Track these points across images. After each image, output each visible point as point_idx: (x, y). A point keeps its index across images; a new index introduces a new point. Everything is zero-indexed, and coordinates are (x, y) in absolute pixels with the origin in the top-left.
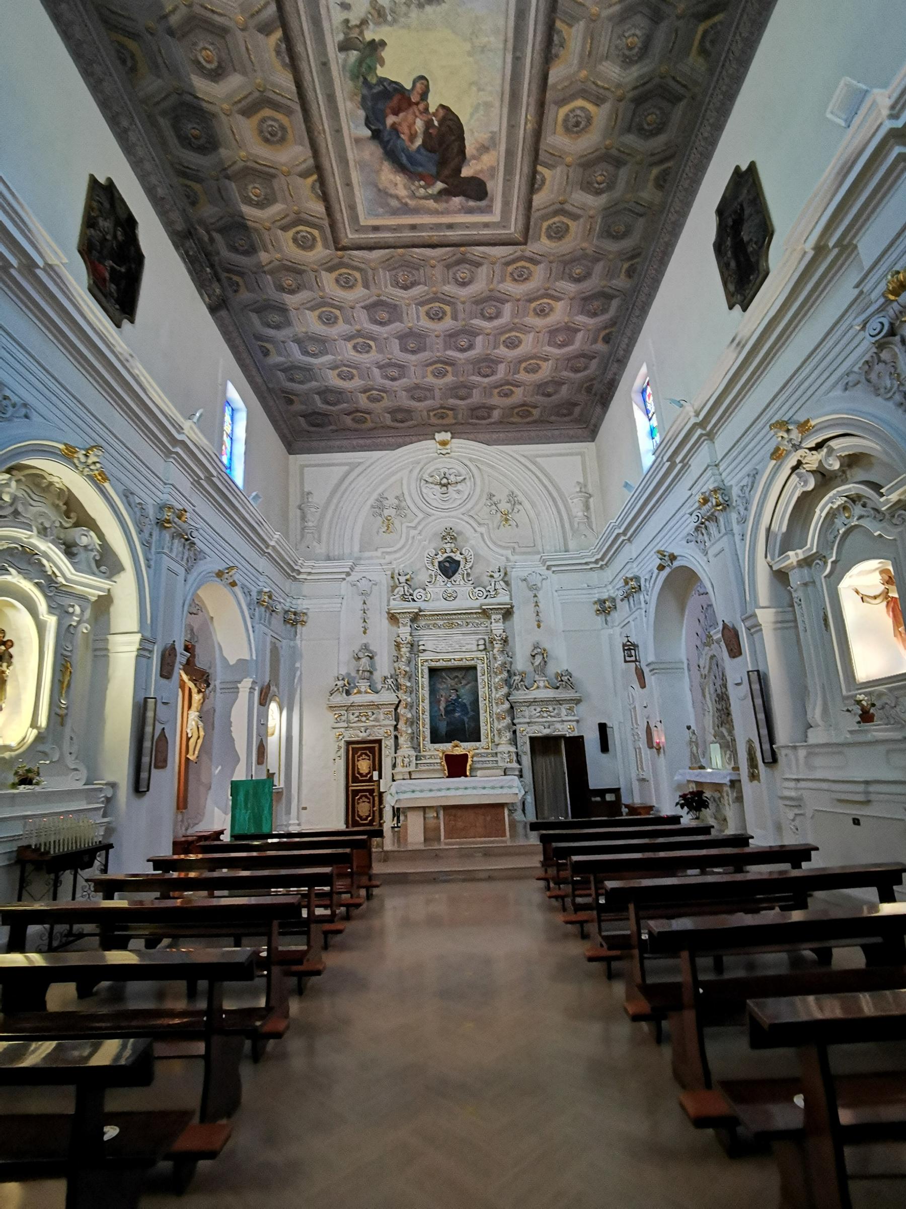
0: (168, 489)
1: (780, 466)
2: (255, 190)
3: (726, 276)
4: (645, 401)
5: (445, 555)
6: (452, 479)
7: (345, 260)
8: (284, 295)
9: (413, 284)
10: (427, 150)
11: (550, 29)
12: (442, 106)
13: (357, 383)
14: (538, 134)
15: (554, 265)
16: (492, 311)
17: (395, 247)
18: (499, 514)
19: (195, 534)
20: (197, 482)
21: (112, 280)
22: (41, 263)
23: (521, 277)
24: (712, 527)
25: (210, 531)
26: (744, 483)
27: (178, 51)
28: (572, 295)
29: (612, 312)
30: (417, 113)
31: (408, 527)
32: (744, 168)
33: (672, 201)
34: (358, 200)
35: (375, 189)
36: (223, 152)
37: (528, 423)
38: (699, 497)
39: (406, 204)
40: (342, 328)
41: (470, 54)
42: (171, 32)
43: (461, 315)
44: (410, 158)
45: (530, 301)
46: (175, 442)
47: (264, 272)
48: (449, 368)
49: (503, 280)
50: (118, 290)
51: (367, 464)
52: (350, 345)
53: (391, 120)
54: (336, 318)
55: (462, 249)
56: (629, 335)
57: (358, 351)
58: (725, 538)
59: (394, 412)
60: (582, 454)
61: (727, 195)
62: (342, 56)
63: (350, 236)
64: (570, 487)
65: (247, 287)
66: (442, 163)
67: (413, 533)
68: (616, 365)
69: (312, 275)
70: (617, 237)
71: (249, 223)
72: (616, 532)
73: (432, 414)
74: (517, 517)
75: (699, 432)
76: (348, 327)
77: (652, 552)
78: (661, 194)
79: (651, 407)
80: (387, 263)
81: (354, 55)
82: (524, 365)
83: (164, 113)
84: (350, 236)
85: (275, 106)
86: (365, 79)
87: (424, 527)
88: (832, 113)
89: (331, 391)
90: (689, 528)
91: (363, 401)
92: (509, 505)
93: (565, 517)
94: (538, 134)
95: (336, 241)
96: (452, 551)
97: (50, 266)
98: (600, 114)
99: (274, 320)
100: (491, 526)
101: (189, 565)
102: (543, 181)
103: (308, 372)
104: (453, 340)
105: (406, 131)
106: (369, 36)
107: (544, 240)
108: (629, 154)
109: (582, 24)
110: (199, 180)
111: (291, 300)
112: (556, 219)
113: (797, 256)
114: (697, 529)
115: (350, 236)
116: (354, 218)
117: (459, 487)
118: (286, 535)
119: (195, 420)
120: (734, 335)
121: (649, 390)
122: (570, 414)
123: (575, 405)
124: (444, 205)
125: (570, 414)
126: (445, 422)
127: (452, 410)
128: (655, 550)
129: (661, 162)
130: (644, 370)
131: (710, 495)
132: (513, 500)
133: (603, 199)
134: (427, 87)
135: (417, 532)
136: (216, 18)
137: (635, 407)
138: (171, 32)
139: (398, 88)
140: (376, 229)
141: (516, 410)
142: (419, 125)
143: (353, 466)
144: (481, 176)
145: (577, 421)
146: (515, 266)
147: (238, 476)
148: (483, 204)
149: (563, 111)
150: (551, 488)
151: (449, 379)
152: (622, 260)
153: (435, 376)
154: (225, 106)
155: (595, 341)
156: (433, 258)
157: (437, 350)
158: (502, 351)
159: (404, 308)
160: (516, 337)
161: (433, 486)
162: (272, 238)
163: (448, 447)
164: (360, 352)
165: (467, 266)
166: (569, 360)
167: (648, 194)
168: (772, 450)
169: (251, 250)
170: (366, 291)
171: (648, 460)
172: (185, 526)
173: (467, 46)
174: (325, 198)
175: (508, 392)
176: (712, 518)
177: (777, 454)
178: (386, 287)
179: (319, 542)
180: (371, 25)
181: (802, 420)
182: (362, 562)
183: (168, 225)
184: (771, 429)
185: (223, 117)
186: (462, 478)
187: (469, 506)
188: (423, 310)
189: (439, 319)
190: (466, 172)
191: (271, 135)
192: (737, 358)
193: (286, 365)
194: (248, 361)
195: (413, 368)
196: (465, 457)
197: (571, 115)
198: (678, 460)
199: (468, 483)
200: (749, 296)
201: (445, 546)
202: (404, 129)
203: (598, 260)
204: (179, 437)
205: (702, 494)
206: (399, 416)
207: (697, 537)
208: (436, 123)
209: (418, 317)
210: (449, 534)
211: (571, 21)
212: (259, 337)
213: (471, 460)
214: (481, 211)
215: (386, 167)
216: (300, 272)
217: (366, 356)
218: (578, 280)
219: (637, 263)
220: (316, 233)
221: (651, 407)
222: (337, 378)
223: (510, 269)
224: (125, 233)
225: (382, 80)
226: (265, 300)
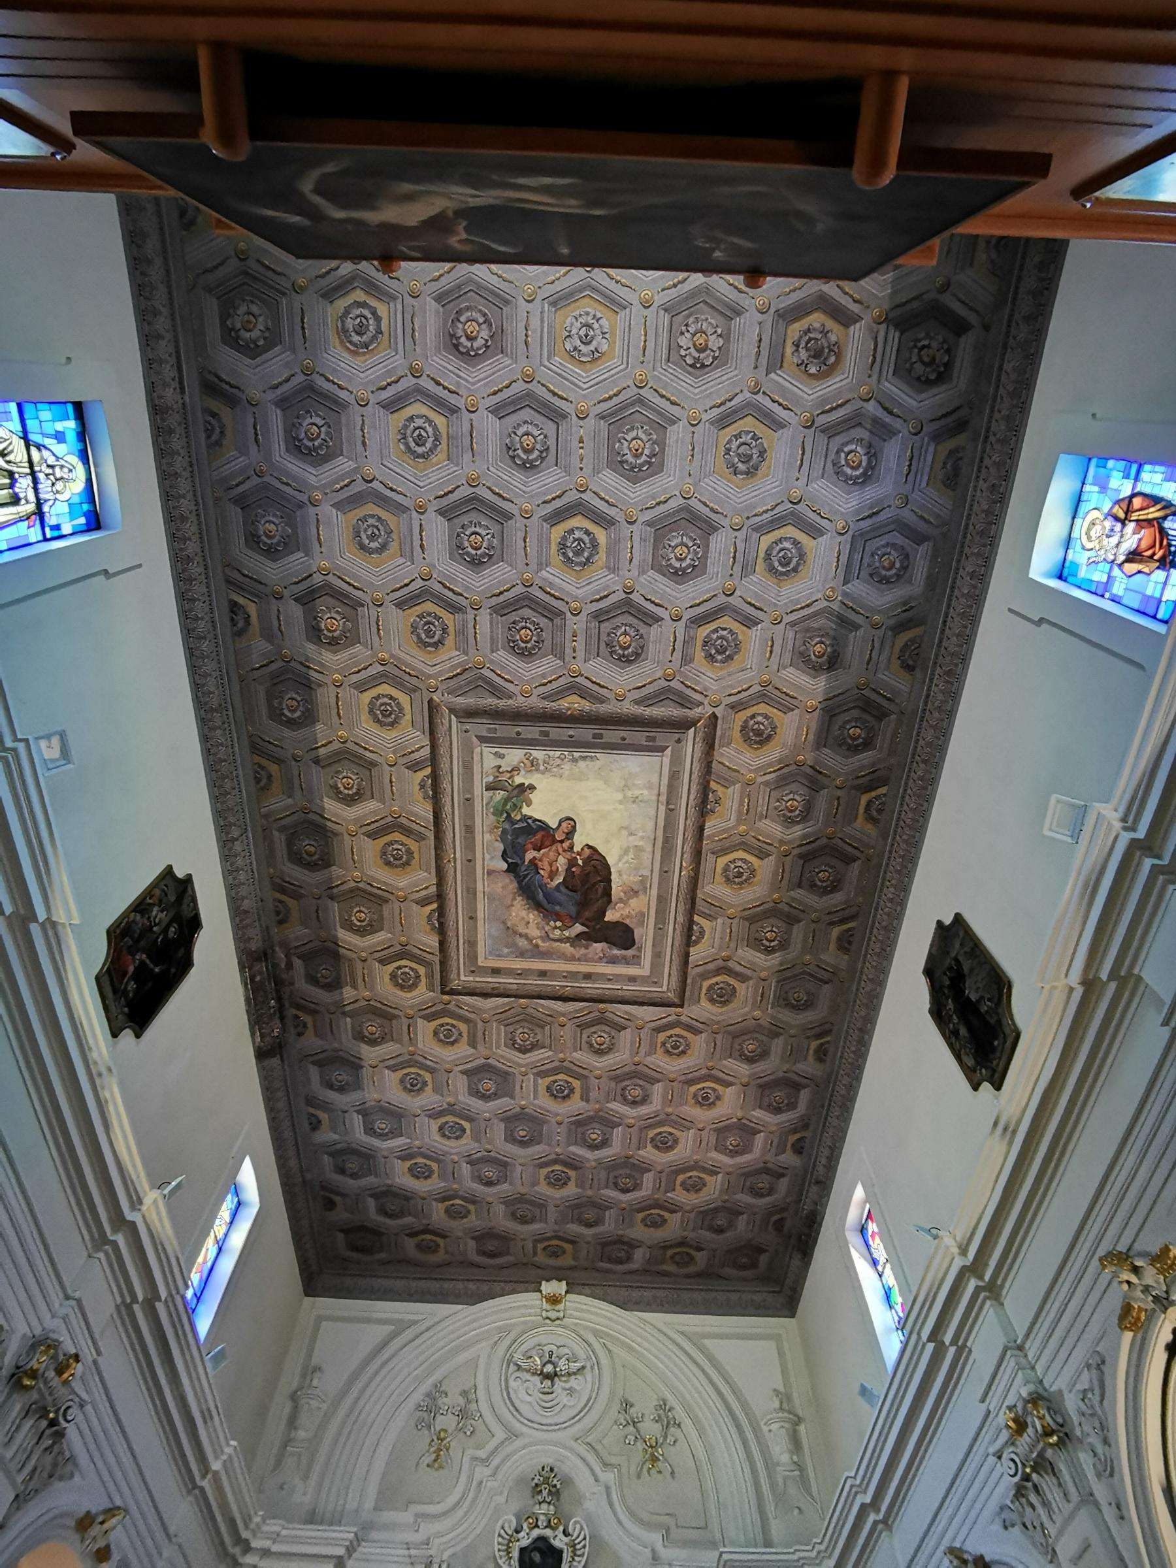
0: (69, 1308)
1: (1144, 1339)
2: (360, 915)
3: (957, 1046)
4: (868, 1246)
5: (536, 1533)
6: (562, 1365)
7: (451, 1007)
8: (363, 1046)
9: (535, 1046)
10: (567, 888)
11: (705, 790)
12: (589, 847)
13: (434, 1185)
14: (694, 882)
15: (719, 1037)
16: (638, 1092)
17: (516, 996)
18: (640, 1445)
19: (73, 1413)
20: (125, 1309)
21: (135, 977)
22: (42, 916)
23: (677, 1050)
24: (1046, 1482)
25: (109, 1421)
26: (1083, 1384)
27: (318, 777)
28: (745, 1080)
29: (802, 1108)
30: (560, 850)
31: (474, 1459)
32: (948, 921)
33: (862, 968)
34: (480, 936)
35: (502, 926)
36: (335, 871)
37: (687, 1276)
38: (1004, 1418)
39: (537, 946)
40: (429, 1099)
41: (621, 802)
42: (317, 761)
43: (593, 1095)
44: (547, 895)
45: (691, 1082)
46: (119, 1220)
47: (344, 1013)
48: (572, 1173)
49: (652, 1051)
50: (136, 992)
51: (427, 1324)
52: (435, 1125)
53: (530, 855)
54: (425, 1083)
55: (602, 1006)
56: (829, 1143)
57: (444, 1136)
58: (1083, 1516)
59: (483, 1237)
60: (777, 1338)
61: (933, 951)
62: (487, 794)
63: (462, 977)
64: (764, 1403)
65: (315, 1031)
66: (583, 905)
67: (482, 1472)
68: (814, 1188)
69: (405, 1021)
70: (797, 1007)
71: (342, 951)
72: (860, 1500)
73: (540, 1246)
74: (670, 1451)
75: (972, 1284)
76: (438, 1098)
77: (939, 1553)
78: (846, 957)
79: (880, 1253)
80: (503, 1017)
81: (500, 795)
82: (681, 1178)
83: (282, 829)
84: (462, 977)
85: (407, 832)
86: (509, 815)
87: (503, 1461)
88: (1051, 830)
89: (395, 1195)
90: (1000, 1490)
91: (438, 1214)
92: (658, 1426)
93: (760, 1465)
94: (694, 882)
95: (444, 981)
96: (549, 1526)
97: (54, 924)
98: (765, 868)
99: (340, 1078)
100: (624, 1470)
101: (32, 1485)
102: (702, 933)
103: (367, 1159)
104: (580, 1130)
105: (547, 867)
106: (518, 780)
107: (704, 1002)
108: (803, 911)
109: (738, 786)
110: (297, 896)
111: (369, 1054)
112: (718, 979)
113: (1059, 997)
114: (1020, 1492)
115: (463, 978)
116: (472, 956)
117: (573, 1382)
118: (249, 1452)
119: (166, 1191)
120: (995, 1115)
121: (872, 1227)
122: (754, 1265)
123: (761, 1251)
124: (583, 951)
125: (754, 1265)
126: (559, 1262)
127: (572, 1242)
128: (942, 1548)
129: (843, 921)
130: (859, 1193)
131: (1025, 1409)
132: (666, 1418)
133: (775, 959)
134: (574, 827)
135: (488, 1471)
136: (368, 754)
137: (855, 1255)
138: (317, 761)
139: (543, 827)
140: (496, 971)
141: (670, 1252)
142: (562, 862)
143: (401, 1326)
144: (627, 921)
145: (766, 1279)
146: (669, 1033)
147: (203, 1324)
148: (630, 953)
149: (722, 861)
150: (730, 1398)
151: (571, 1190)
152: (808, 1037)
153: (550, 1184)
154: (352, 828)
155: (781, 1150)
156: (564, 1015)
157: (558, 1144)
158: (649, 1153)
159: (519, 1078)
160: (659, 1215)
161: (528, 1376)
162: (366, 972)
163: (561, 1306)
164: (449, 1138)
165: (607, 1029)
166: (746, 1175)
167: (831, 956)
168: (1118, 1312)
169: (334, 985)
170: (472, 1051)
171: (891, 1345)
172: (62, 1392)
173: (619, 796)
174: (442, 930)
175: (658, 1219)
176: (1041, 1465)
177: (1127, 1317)
178: (498, 1047)
179: (306, 1477)
180: (523, 772)
181: (1155, 1249)
182: (374, 1535)
183: (240, 939)
184: (1104, 1267)
185: (346, 837)
186: (578, 1365)
187: (588, 1421)
188: (543, 1083)
189: (564, 1098)
190: (610, 916)
191: (395, 859)
192: (1008, 1152)
193: (338, 1147)
194: (287, 1134)
195: (519, 1168)
196: (586, 1328)
197: (752, 722)
198: (947, 1339)
199: (589, 1377)
200: (1000, 1068)
201: (536, 1509)
202: (545, 865)
203: (777, 1035)
204: (130, 1216)
205: (1010, 1408)
206: (490, 1246)
207: (1022, 1515)
208: (580, 862)
209: (536, 1092)
210: (546, 1480)
211: (727, 783)
212: (311, 1101)
213: (596, 1333)
214: (626, 961)
215: (519, 902)
216: (391, 1018)
217: (453, 1143)
218: (751, 1060)
219: (828, 1042)
220: (422, 970)
221: (880, 1253)
222: (408, 1175)
223: (662, 1037)
224: (180, 931)
225: (525, 818)
226: (335, 1050)
